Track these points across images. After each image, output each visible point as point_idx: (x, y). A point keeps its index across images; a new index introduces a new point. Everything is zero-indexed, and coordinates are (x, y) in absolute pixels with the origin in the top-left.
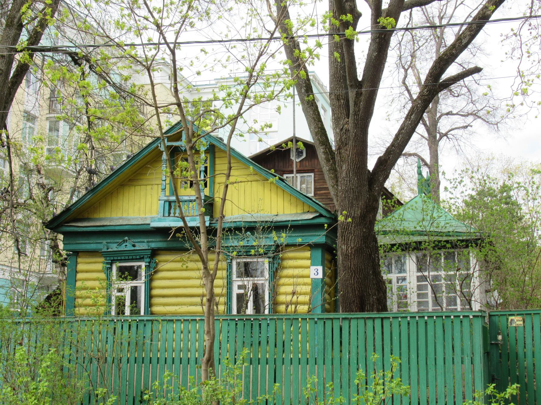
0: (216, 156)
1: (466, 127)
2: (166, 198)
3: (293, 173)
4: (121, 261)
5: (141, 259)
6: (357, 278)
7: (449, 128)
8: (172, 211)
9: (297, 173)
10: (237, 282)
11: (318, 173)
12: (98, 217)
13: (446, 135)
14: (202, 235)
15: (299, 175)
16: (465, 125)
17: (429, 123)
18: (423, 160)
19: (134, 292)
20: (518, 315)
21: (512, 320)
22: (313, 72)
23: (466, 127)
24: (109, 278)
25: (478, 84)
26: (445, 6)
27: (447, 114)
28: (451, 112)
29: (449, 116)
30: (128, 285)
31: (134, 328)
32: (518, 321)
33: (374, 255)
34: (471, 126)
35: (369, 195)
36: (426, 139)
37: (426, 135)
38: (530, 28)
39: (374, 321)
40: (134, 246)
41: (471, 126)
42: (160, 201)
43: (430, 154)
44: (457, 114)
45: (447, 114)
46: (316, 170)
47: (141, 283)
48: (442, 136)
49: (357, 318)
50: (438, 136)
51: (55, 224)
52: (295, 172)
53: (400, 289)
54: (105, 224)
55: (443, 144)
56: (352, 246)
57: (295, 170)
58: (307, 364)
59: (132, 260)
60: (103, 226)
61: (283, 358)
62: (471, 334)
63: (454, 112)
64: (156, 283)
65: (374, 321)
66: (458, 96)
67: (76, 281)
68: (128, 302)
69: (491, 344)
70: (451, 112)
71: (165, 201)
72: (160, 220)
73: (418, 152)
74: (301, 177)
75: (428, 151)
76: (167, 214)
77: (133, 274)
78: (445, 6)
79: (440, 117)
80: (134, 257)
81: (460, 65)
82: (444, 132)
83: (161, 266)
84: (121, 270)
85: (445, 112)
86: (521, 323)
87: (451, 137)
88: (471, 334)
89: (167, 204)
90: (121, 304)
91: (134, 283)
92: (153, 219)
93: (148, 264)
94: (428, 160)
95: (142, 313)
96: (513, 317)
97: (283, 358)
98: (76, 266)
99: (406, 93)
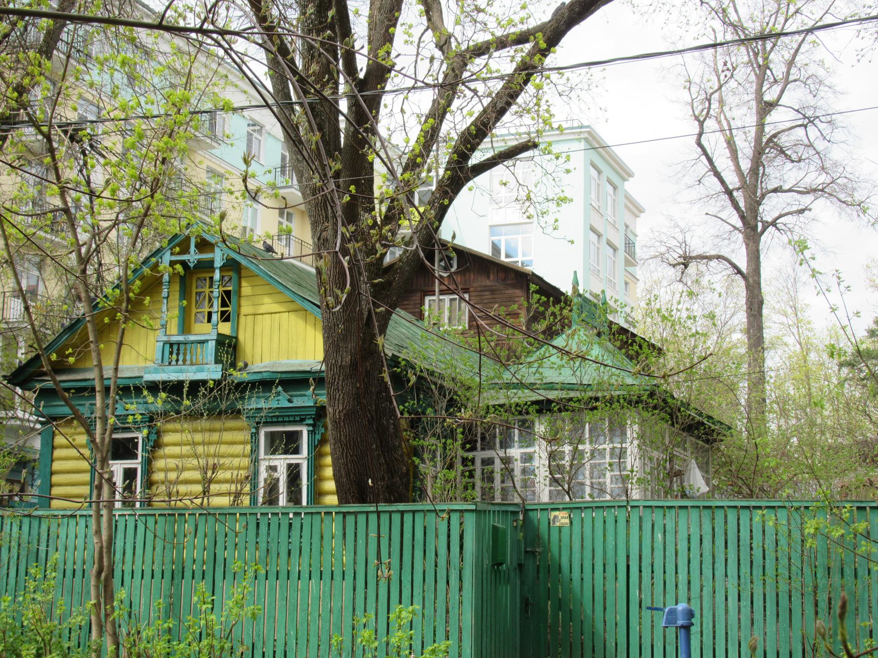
0: (243, 275)
1: (801, 211)
2: (165, 339)
3: (434, 295)
4: (273, 423)
5: (301, 421)
6: (351, 456)
7: (777, 215)
8: (181, 357)
9: (441, 294)
10: (266, 461)
11: (474, 294)
12: (82, 367)
13: (774, 223)
14: (97, 394)
15: (447, 298)
16: (801, 207)
17: (745, 206)
18: (734, 266)
19: (294, 473)
20: (564, 509)
21: (555, 517)
22: (588, 127)
23: (801, 211)
24: (255, 450)
25: (829, 141)
26: (774, 16)
27: (775, 190)
28: (781, 187)
29: (779, 194)
30: (281, 462)
31: (263, 528)
32: (562, 518)
33: (387, 421)
34: (810, 210)
35: (364, 334)
36: (740, 231)
37: (739, 224)
38: (725, 68)
39: (356, 517)
40: (290, 401)
41: (810, 210)
42: (158, 344)
43: (748, 255)
44: (790, 190)
45: (775, 190)
46: (471, 289)
47: (302, 459)
48: (766, 225)
49: (312, 513)
50: (760, 225)
51: (21, 378)
52: (437, 293)
53: (524, 471)
54: (88, 377)
55: (769, 239)
56: (341, 408)
57: (437, 290)
58: (277, 579)
59: (290, 423)
60: (85, 380)
61: (204, 571)
62: (628, 535)
63: (786, 187)
64: (160, 464)
65: (356, 517)
66: (799, 161)
67: (52, 461)
68: (282, 487)
69: (526, 552)
70: (781, 187)
71: (165, 343)
72: (156, 371)
73: (724, 253)
74: (451, 300)
75: (743, 251)
76: (174, 363)
77: (290, 444)
78: (774, 16)
79: (763, 196)
80: (286, 419)
81: (797, 111)
82: (770, 220)
83: (167, 438)
84: (272, 438)
85: (770, 187)
86: (567, 521)
87: (783, 227)
88: (628, 535)
89: (167, 347)
90: (272, 489)
91: (293, 459)
92: (146, 370)
93: (311, 428)
94: (743, 266)
95: (304, 503)
96: (557, 513)
97: (204, 571)
98: (53, 439)
99: (703, 158)
